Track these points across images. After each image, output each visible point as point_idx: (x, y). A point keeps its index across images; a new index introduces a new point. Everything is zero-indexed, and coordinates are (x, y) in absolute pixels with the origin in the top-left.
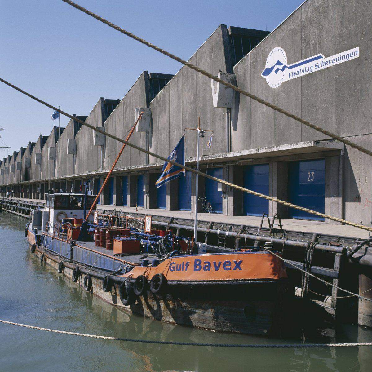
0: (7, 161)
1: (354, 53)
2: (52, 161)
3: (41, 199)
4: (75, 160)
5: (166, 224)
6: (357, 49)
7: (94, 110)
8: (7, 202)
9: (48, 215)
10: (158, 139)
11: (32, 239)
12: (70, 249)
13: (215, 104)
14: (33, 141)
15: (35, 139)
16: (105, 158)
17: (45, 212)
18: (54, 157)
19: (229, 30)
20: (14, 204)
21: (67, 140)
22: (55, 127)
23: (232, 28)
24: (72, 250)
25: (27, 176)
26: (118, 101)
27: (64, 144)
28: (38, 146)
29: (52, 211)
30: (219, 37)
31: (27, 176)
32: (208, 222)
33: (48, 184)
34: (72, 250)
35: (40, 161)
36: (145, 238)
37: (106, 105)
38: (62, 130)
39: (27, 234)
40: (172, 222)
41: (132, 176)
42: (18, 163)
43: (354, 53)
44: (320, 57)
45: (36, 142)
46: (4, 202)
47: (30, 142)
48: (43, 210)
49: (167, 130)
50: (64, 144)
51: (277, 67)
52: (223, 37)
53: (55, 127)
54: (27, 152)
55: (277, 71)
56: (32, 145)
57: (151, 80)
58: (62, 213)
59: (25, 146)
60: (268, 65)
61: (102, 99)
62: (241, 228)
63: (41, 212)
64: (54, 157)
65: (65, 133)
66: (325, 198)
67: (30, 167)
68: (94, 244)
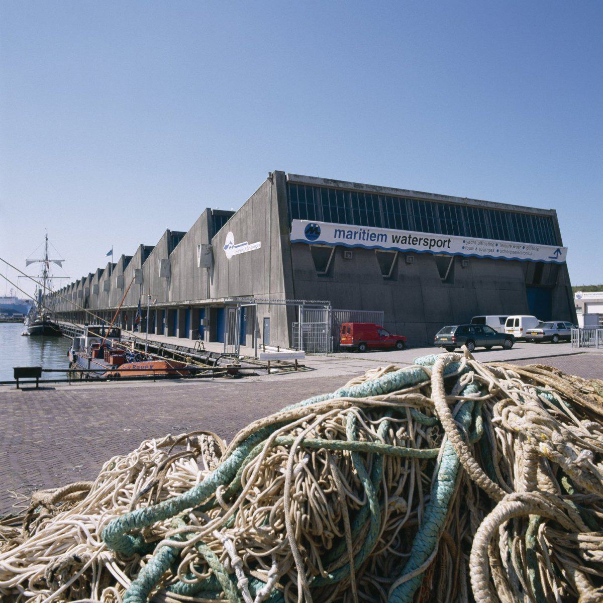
0: (76, 286)
1: (257, 245)
2: (106, 293)
3: (157, 334)
4: (108, 296)
5: (205, 358)
6: (259, 243)
7: (136, 253)
8: (66, 328)
9: (84, 340)
10: (174, 284)
11: (71, 358)
12: (88, 363)
13: (199, 266)
14: (128, 254)
15: (132, 250)
16: (212, 284)
17: (82, 339)
18: (107, 290)
19: (287, 176)
20: (72, 330)
21: (199, 246)
22: (109, 263)
23: (214, 211)
24: (89, 364)
25: (86, 303)
26: (184, 234)
27: (155, 264)
28: (96, 277)
29: (87, 338)
30: (205, 216)
31: (86, 303)
32: (175, 346)
33: (146, 311)
34: (89, 364)
35: (97, 292)
36: (129, 355)
37: (145, 250)
38: (114, 265)
39: (68, 355)
40: (211, 356)
41: (181, 309)
42: (79, 291)
43: (257, 245)
44: (246, 244)
45: (154, 244)
46: (64, 328)
47: (99, 269)
48: (80, 337)
49: (178, 278)
50: (155, 264)
51: (230, 245)
52: (208, 217)
53: (109, 263)
54: (87, 282)
55: (230, 247)
56: (92, 276)
57: (213, 216)
58: (94, 340)
59: (86, 276)
60: (227, 243)
61: (142, 245)
62: (187, 349)
63: (79, 339)
64: (107, 290)
65: (117, 268)
66: (247, 335)
67: (89, 295)
68: (104, 360)
